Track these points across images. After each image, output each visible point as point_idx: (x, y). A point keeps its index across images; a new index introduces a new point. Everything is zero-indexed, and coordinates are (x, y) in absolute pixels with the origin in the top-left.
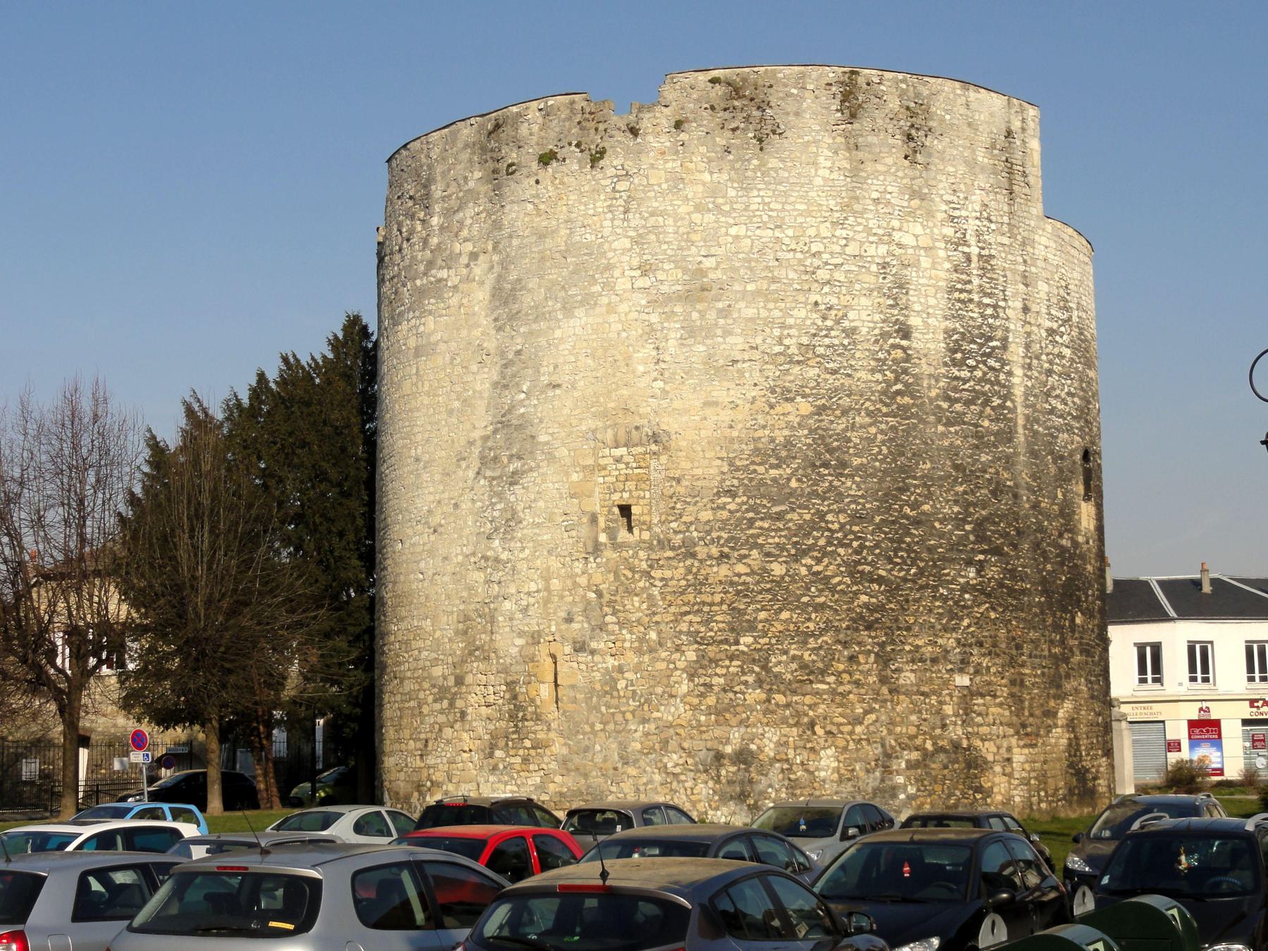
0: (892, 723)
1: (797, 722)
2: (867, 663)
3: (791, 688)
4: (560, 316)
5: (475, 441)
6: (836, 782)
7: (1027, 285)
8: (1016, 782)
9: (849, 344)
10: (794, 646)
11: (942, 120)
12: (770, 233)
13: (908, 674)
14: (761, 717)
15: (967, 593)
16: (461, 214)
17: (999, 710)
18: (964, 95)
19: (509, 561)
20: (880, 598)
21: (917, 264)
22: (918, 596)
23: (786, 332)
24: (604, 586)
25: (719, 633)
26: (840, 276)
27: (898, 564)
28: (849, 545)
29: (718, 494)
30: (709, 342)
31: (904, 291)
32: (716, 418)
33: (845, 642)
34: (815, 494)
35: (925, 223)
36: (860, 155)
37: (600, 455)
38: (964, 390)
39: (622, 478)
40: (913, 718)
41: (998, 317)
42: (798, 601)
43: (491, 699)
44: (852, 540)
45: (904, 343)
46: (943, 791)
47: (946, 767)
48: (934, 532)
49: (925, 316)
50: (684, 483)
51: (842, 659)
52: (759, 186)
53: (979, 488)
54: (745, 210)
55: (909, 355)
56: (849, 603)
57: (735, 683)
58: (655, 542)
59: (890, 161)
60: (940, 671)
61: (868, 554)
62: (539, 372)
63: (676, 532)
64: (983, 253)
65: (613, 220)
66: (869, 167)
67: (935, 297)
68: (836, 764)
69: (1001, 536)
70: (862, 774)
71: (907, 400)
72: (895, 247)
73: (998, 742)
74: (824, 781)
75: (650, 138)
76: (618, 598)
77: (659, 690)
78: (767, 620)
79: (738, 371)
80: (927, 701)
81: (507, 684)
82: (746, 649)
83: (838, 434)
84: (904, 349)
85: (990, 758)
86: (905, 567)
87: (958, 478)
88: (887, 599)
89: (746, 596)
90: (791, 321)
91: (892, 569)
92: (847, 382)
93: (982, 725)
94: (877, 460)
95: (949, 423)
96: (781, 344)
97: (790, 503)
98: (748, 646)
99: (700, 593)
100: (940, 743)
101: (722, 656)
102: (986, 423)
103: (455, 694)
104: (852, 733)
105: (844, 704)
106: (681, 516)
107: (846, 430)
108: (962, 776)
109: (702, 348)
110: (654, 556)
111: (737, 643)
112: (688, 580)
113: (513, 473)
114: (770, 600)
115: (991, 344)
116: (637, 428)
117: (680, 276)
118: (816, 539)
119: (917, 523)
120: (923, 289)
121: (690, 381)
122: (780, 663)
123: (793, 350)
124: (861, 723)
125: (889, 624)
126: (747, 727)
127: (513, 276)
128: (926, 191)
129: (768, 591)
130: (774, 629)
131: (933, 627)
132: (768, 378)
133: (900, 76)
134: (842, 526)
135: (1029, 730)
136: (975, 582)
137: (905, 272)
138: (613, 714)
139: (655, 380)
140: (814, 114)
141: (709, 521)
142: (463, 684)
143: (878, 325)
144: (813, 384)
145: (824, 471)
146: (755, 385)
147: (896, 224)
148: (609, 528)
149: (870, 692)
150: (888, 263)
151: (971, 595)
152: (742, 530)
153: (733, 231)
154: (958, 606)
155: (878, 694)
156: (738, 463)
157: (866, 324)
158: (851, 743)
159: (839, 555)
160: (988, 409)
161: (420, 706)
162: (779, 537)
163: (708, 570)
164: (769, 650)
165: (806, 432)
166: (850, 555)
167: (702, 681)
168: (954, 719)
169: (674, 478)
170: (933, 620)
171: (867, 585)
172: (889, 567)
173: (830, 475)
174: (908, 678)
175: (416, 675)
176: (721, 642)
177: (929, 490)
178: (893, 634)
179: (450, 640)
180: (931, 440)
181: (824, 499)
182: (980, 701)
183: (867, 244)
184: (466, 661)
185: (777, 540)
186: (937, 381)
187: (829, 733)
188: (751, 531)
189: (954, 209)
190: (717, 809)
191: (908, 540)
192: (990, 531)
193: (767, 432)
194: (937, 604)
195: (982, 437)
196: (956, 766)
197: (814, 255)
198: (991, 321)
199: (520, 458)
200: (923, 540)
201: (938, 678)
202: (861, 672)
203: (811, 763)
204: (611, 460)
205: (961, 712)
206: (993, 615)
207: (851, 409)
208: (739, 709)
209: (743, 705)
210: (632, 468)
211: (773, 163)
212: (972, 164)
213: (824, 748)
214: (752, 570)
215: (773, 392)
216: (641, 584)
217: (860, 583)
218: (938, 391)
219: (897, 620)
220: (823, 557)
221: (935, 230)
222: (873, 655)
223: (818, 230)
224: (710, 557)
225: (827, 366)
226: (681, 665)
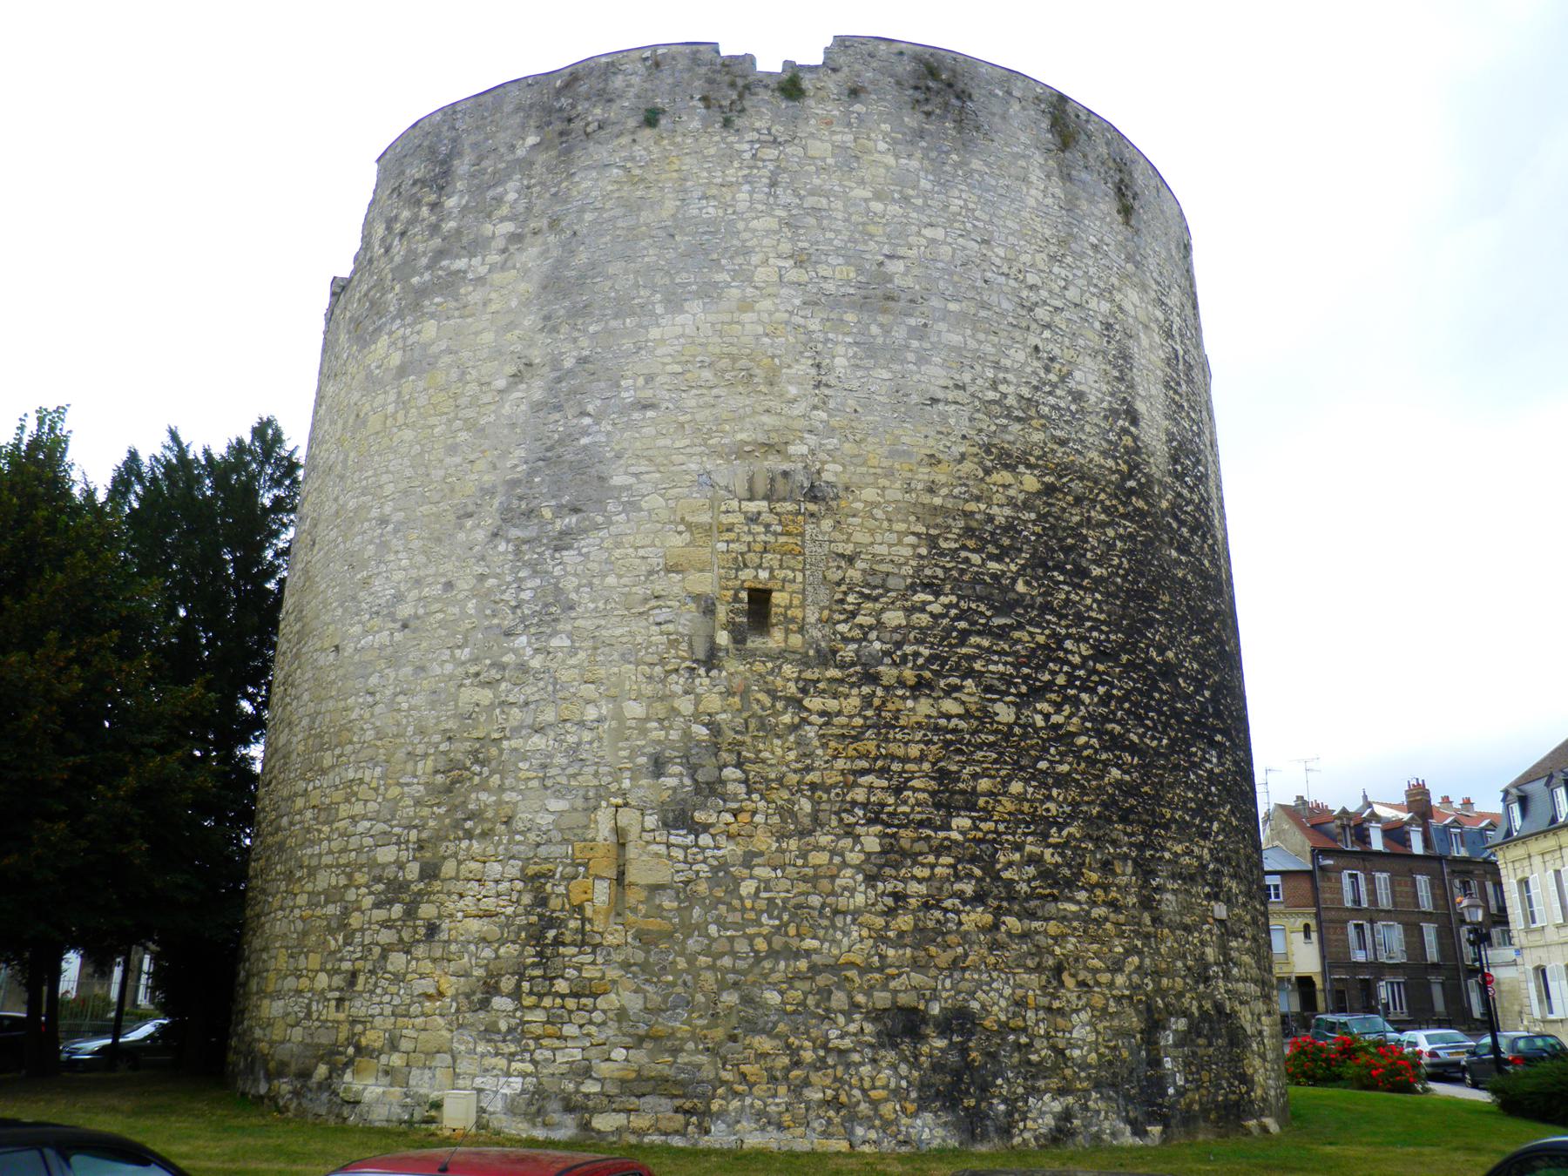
1: (1039, 964)
2: (1124, 874)
4: (659, 309)
5: (494, 487)
10: (1030, 839)
14: (984, 952)
16: (500, 189)
19: (547, 670)
23: (1001, 375)
24: (724, 716)
25: (918, 809)
29: (913, 588)
37: (723, 508)
39: (758, 547)
42: (1034, 766)
43: (489, 904)
50: (859, 564)
56: (1097, 777)
58: (811, 653)
62: (619, 386)
63: (845, 640)
65: (751, 193)
75: (811, 103)
76: (748, 739)
77: (815, 901)
78: (990, 794)
79: (940, 414)
81: (525, 878)
82: (960, 838)
83: (1072, 528)
89: (959, 752)
90: (1006, 362)
96: (996, 389)
97: (1018, 615)
98: (963, 833)
99: (887, 740)
103: (420, 893)
106: (853, 614)
107: (1080, 524)
109: (886, 375)
110: (808, 675)
112: (866, 718)
113: (561, 533)
114: (995, 761)
116: (785, 474)
117: (852, 275)
121: (870, 418)
122: (1010, 864)
123: (1011, 401)
124: (1121, 970)
127: (582, 257)
129: (991, 745)
130: (1000, 808)
132: (981, 430)
134: (1085, 659)
138: (731, 939)
139: (815, 408)
141: (899, 627)
142: (436, 877)
144: (1037, 453)
148: (734, 624)
153: (928, 232)
156: (944, 545)
161: (346, 913)
162: (1005, 664)
163: (899, 704)
164: (996, 841)
165: (1033, 516)
167: (889, 888)
169: (842, 556)
172: (1141, 730)
174: (1169, 902)
175: (342, 861)
176: (921, 824)
179: (418, 803)
184: (446, 838)
185: (1001, 668)
188: (964, 650)
190: (915, 1115)
199: (576, 510)
202: (1119, 888)
204: (741, 518)
208: (952, 939)
210: (775, 534)
213: (1077, 1011)
214: (967, 711)
215: (988, 452)
216: (787, 719)
222: (1130, 863)
224: (902, 683)
226: (854, 858)
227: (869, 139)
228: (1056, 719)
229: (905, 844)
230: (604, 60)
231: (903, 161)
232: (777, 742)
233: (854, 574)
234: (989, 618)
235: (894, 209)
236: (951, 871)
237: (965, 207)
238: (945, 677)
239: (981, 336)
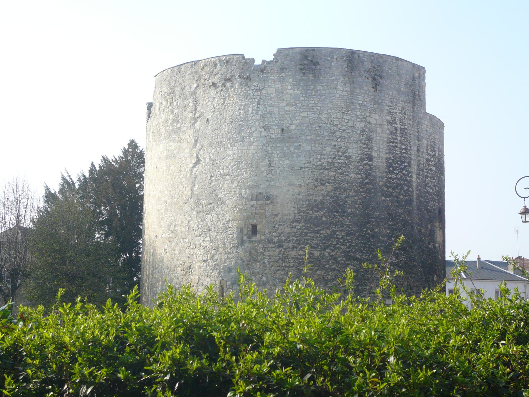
9: (348, 162)
23: (322, 157)
29: (293, 222)
34: (332, 223)
42: (324, 266)
49: (378, 152)
50: (279, 216)
58: (266, 241)
63: (275, 237)
66: (358, 90)
71: (370, 186)
83: (342, 199)
84: (370, 165)
90: (324, 152)
91: (362, 255)
92: (347, 178)
94: (357, 210)
96: (320, 161)
99: (284, 262)
102: (401, 197)
106: (277, 230)
107: (345, 198)
109: (288, 162)
112: (279, 257)
116: (260, 193)
118: (332, 242)
119: (373, 236)
123: (325, 164)
128: (380, 101)
132: (315, 175)
139: (269, 174)
141: (289, 233)
144: (333, 178)
146: (309, 178)
147: (368, 114)
150: (364, 130)
151: (393, 267)
152: (302, 237)
156: (302, 210)
157: (355, 154)
159: (341, 248)
169: (275, 215)
171: (352, 261)
173: (338, 216)
177: (378, 223)
185: (316, 241)
186: (383, 179)
189: (391, 109)
193: (314, 197)
207: (347, 189)
215: (316, 181)
218: (382, 183)
219: (364, 276)
220: (335, 249)
223: (337, 115)
224: (289, 248)
227: (286, 85)
228: (332, 254)
230: (213, 59)
231: (296, 91)
232: (258, 264)
233: (277, 219)
234: (314, 228)
235: (293, 108)
237: (315, 103)
238: (300, 245)
239: (317, 145)
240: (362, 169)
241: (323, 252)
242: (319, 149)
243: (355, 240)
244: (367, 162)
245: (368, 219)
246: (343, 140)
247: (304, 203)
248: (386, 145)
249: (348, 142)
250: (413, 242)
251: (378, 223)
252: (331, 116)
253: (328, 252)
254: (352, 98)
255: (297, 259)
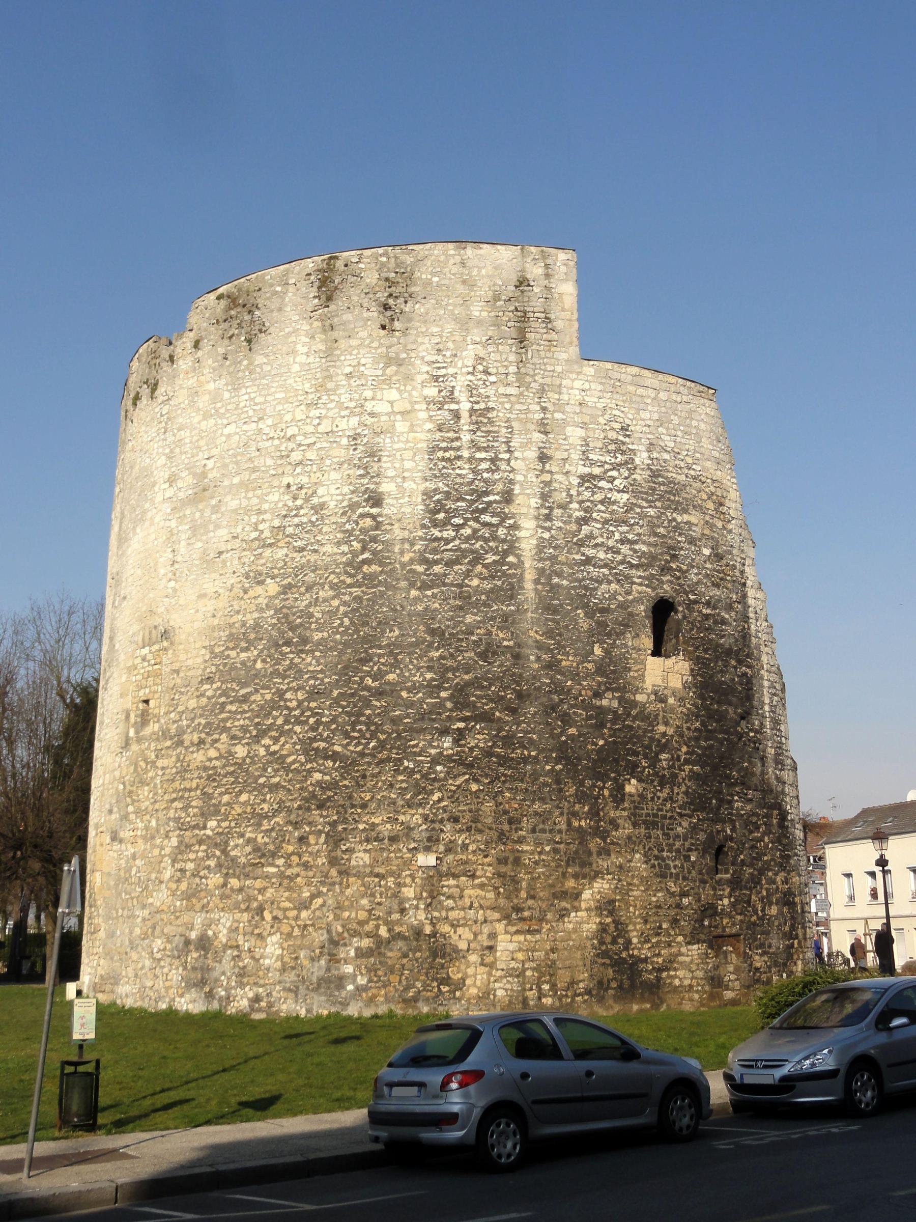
0: (339, 907)
1: (248, 907)
2: (317, 844)
3: (247, 871)
6: (279, 970)
7: (546, 433)
8: (499, 973)
9: (317, 520)
10: (250, 829)
11: (429, 283)
12: (254, 425)
13: (361, 855)
14: (218, 901)
15: (440, 764)
17: (479, 892)
18: (459, 255)
20: (334, 775)
21: (390, 430)
22: (377, 770)
26: (311, 455)
27: (356, 738)
28: (306, 722)
29: (201, 682)
30: (204, 538)
31: (376, 459)
32: (204, 609)
33: (296, 823)
34: (276, 673)
35: (402, 388)
36: (335, 334)
38: (447, 550)
40: (364, 902)
41: (498, 469)
42: (256, 782)
44: (309, 717)
45: (374, 511)
46: (400, 981)
47: (405, 956)
48: (400, 701)
49: (399, 480)
50: (182, 674)
51: (292, 840)
52: (247, 384)
53: (461, 651)
54: (236, 409)
55: (380, 522)
56: (301, 782)
57: (201, 868)
59: (363, 334)
60: (400, 850)
61: (323, 730)
64: (476, 407)
66: (343, 344)
67: (413, 460)
68: (280, 952)
69: (491, 700)
70: (306, 963)
71: (375, 568)
72: (367, 417)
73: (474, 928)
74: (268, 969)
77: (153, 876)
78: (228, 804)
80: (383, 883)
83: (302, 611)
84: (374, 517)
85: (463, 946)
86: (364, 741)
87: (433, 643)
88: (342, 775)
89: (214, 780)
90: (266, 506)
91: (348, 744)
92: (313, 558)
93: (452, 909)
94: (338, 632)
95: (424, 587)
96: (256, 530)
97: (255, 684)
98: (213, 830)
99: (184, 780)
100: (397, 929)
101: (194, 841)
102: (475, 582)
104: (297, 918)
105: (291, 888)
107: (309, 605)
108: (426, 966)
111: (205, 828)
112: (177, 768)
114: (233, 783)
115: (486, 499)
118: (275, 718)
119: (379, 693)
120: (398, 454)
122: (237, 846)
124: (307, 908)
125: (341, 802)
126: (207, 912)
128: (404, 355)
129: (232, 773)
131: (394, 803)
132: (244, 564)
133: (381, 251)
135: (526, 914)
136: (450, 752)
137: (377, 440)
140: (294, 305)
143: (347, 497)
145: (286, 649)
146: (234, 572)
147: (368, 394)
149: (318, 874)
150: (359, 434)
151: (445, 766)
152: (216, 715)
154: (427, 779)
155: (326, 877)
157: (334, 497)
158: (296, 929)
159: (295, 733)
160: (479, 568)
162: (244, 719)
166: (306, 732)
168: (415, 902)
170: (393, 796)
171: (321, 762)
173: (291, 652)
174: (361, 858)
177: (395, 659)
178: (346, 812)
180: (401, 606)
181: (284, 677)
182: (452, 882)
183: (339, 419)
185: (242, 722)
186: (412, 544)
187: (275, 918)
188: (223, 716)
189: (439, 368)
190: (182, 996)
191: (368, 712)
192: (476, 696)
193: (240, 617)
194: (400, 778)
195: (469, 597)
196: (418, 954)
197: (289, 439)
198: (485, 475)
200: (386, 711)
201: (397, 858)
202: (311, 853)
203: (257, 950)
205: (424, 894)
206: (474, 787)
207: (315, 584)
208: (203, 894)
209: (206, 890)
211: (259, 359)
212: (464, 323)
213: (270, 934)
216: (150, 774)
217: (314, 760)
218: (412, 555)
219: (350, 797)
220: (280, 736)
221: (414, 393)
222: (323, 835)
223: (294, 415)
224: (192, 744)
225: (295, 544)
229: (187, 840)
236: (205, 854)
240: (353, 529)
241: (255, 747)
242: (255, 501)
243: (330, 708)
244: (368, 509)
245: (366, 651)
246: (308, 469)
247: (222, 633)
248: (423, 459)
249: (320, 469)
250: (520, 696)
251: (395, 659)
252: (281, 419)
253: (264, 746)
254: (328, 364)
255: (205, 769)
